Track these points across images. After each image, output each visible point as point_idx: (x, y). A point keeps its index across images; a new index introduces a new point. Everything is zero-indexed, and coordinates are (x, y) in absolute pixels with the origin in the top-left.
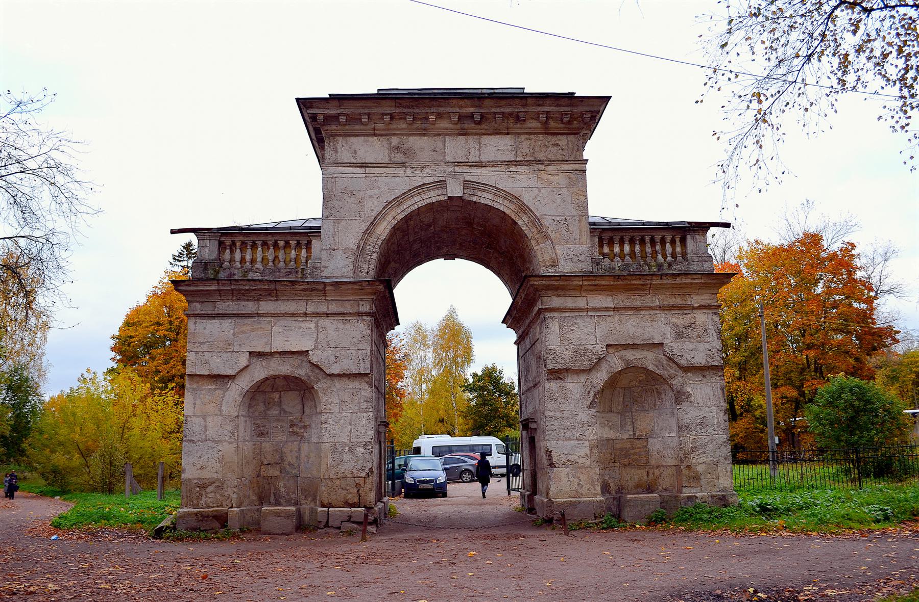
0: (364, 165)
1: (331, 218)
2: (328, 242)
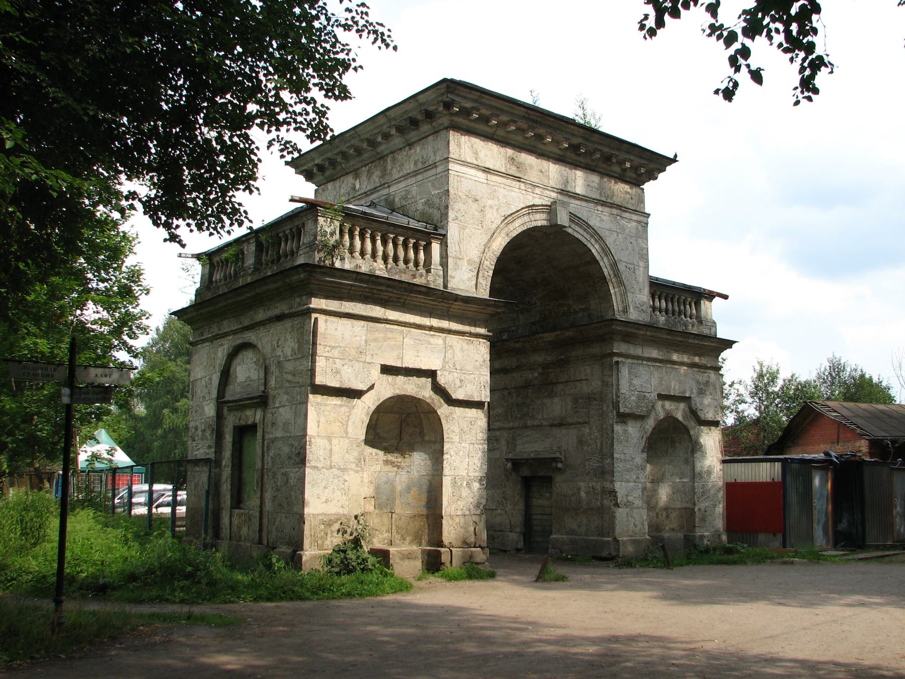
0: (486, 170)
1: (456, 221)
2: (454, 249)
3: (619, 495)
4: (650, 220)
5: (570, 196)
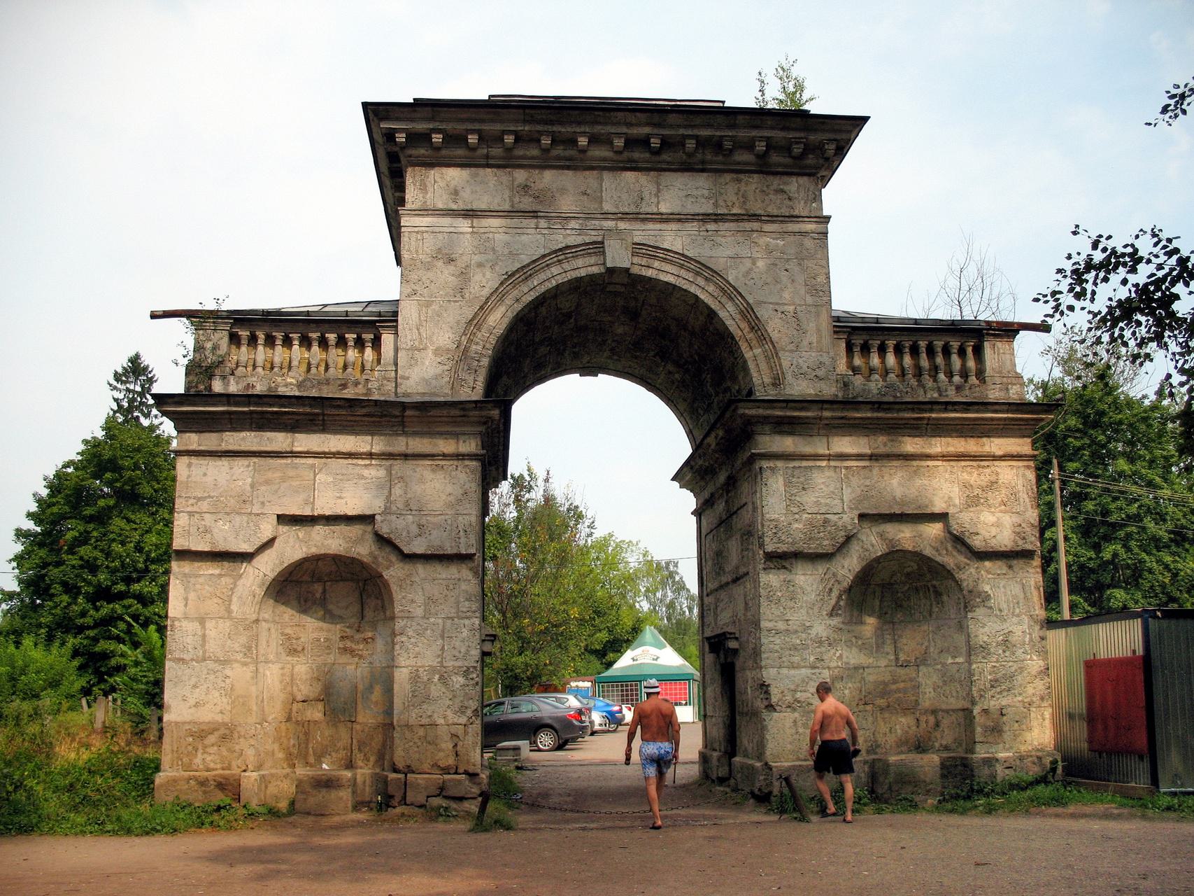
3: (774, 691)
4: (831, 226)
5: (643, 220)
